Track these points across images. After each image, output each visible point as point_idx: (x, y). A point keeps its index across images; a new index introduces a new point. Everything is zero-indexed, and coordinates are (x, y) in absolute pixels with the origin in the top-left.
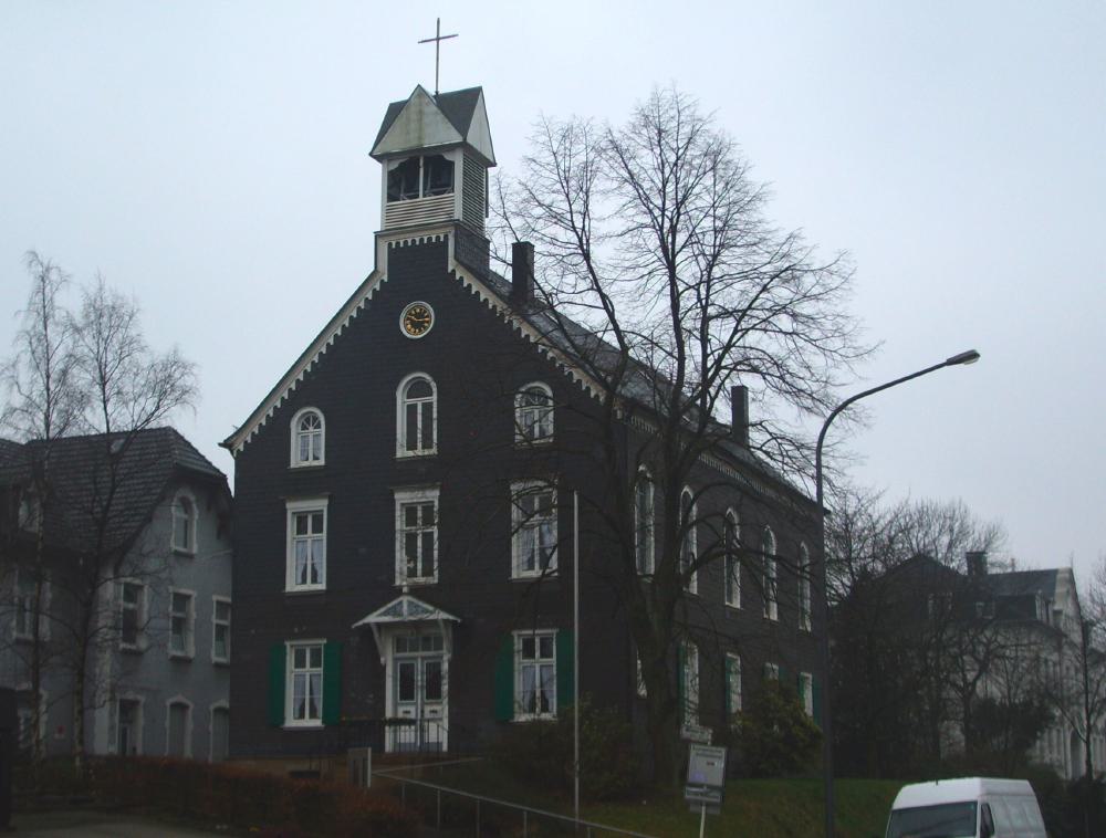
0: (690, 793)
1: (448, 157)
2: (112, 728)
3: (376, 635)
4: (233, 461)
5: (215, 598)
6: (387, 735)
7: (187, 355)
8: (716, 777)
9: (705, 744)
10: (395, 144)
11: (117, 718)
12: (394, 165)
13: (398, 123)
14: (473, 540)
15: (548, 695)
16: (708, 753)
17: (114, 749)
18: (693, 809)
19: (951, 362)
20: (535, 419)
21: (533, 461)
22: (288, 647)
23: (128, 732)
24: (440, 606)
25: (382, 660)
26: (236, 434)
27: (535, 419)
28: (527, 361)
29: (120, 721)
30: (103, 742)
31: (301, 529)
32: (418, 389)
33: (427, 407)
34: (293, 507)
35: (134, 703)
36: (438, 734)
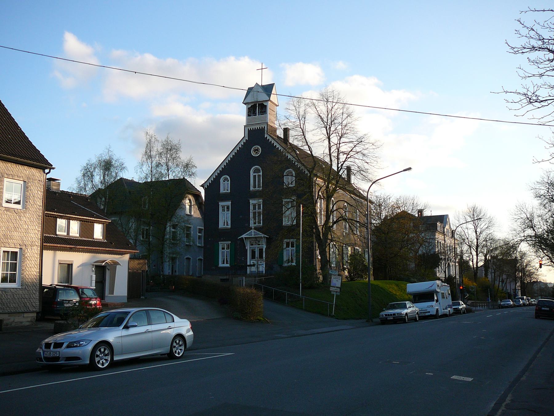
1: (265, 104)
5: (198, 227)
7: (195, 162)
10: (249, 100)
12: (250, 106)
13: (251, 94)
14: (272, 216)
19: (405, 170)
20: (289, 180)
21: (290, 192)
27: (289, 180)
28: (289, 164)
30: (167, 271)
31: (224, 210)
32: (257, 171)
33: (259, 176)
34: (221, 204)
36: (262, 268)
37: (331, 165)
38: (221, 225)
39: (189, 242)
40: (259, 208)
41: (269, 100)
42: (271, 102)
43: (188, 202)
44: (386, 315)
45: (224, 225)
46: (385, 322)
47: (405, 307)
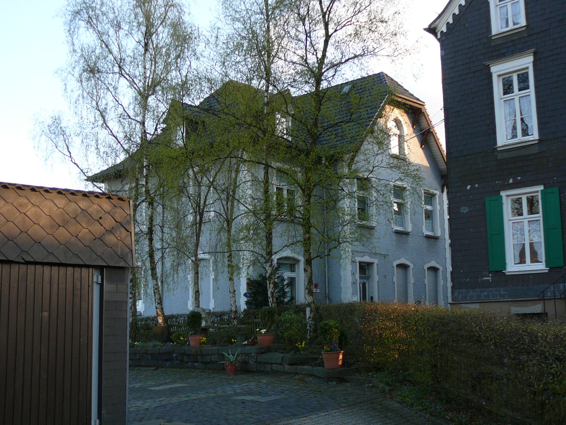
4: (437, 45)
11: (358, 275)
15: (536, 247)
17: (356, 298)
22: (504, 199)
23: (367, 285)
29: (360, 278)
31: (508, 89)
34: (498, 69)
35: (370, 264)
38: (503, 138)
39: (402, 225)
43: (393, 118)
45: (514, 136)
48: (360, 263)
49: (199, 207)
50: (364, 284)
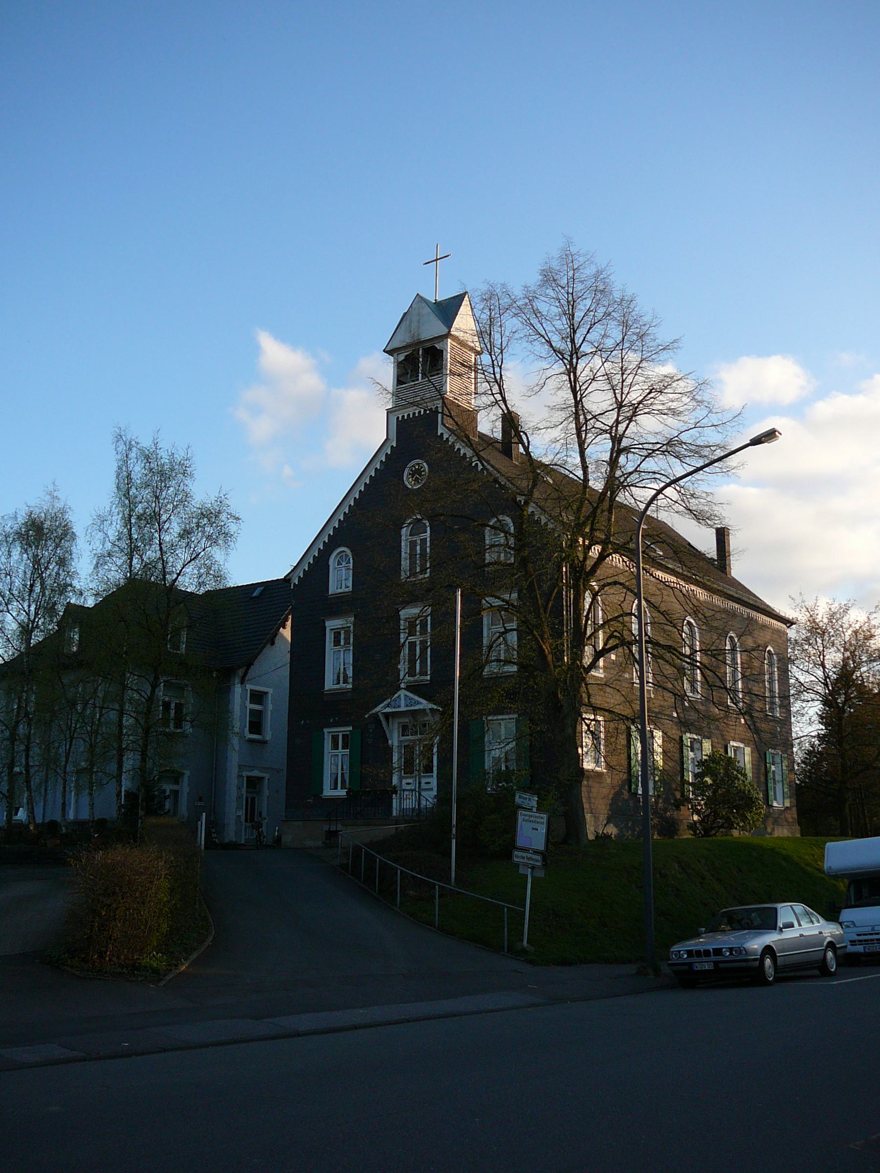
0: (518, 857)
2: (239, 798)
3: (384, 723)
6: (394, 801)
7: (235, 505)
8: (540, 844)
9: (530, 810)
12: (402, 357)
16: (532, 819)
18: (522, 871)
20: (497, 545)
24: (429, 699)
25: (390, 742)
26: (292, 571)
27: (497, 545)
31: (337, 642)
37: (586, 480)
38: (329, 684)
40: (424, 631)
41: (448, 335)
42: (456, 339)
44: (690, 953)
46: (688, 978)
47: (770, 923)
48: (248, 777)
49: (70, 730)
50: (253, 799)
